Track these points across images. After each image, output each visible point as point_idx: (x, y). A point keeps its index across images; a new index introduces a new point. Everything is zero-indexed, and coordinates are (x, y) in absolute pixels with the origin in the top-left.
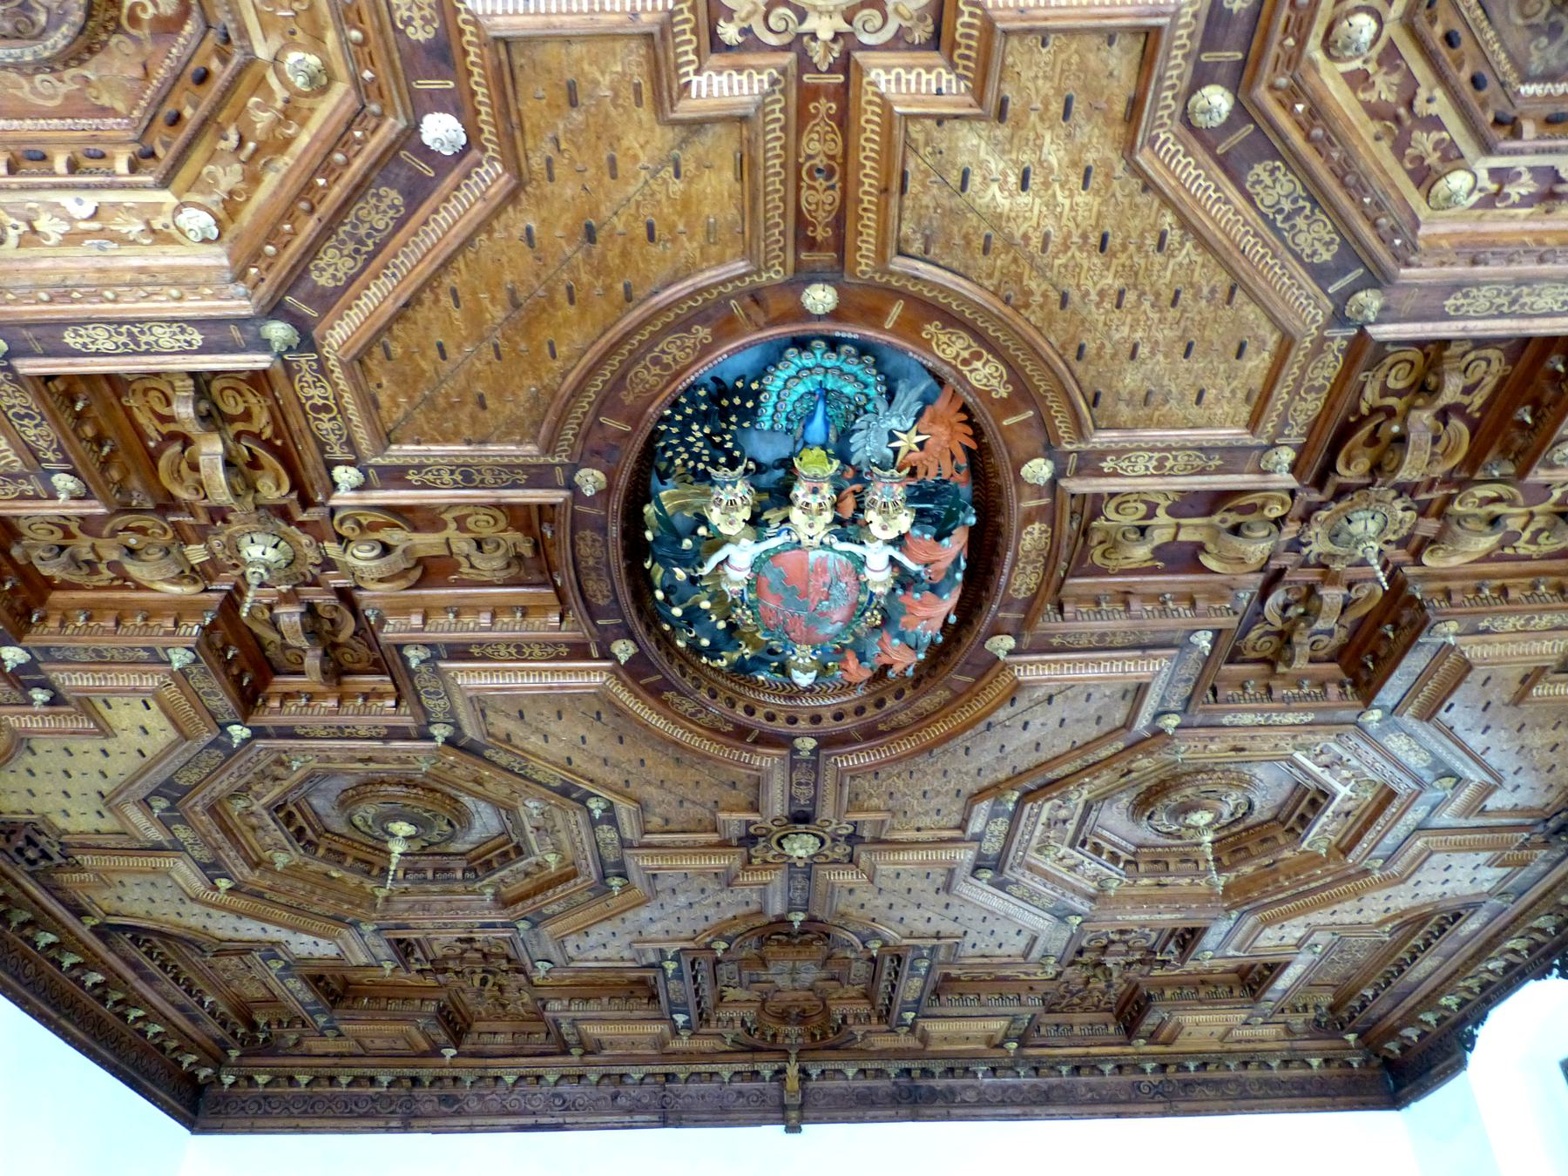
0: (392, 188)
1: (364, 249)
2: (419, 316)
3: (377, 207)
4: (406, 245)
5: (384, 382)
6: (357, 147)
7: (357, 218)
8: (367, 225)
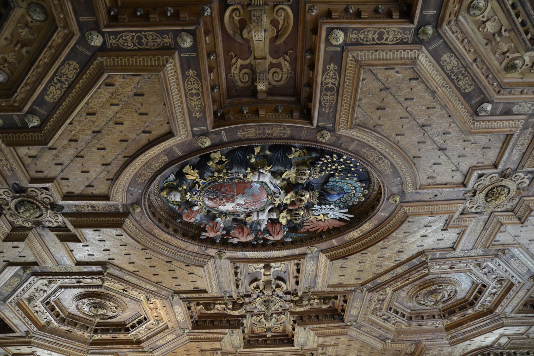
0: (472, 90)
1: (453, 75)
2: (427, 94)
3: (467, 84)
4: (453, 92)
5: (398, 75)
6: (491, 82)
7: (466, 76)
8: (462, 78)
